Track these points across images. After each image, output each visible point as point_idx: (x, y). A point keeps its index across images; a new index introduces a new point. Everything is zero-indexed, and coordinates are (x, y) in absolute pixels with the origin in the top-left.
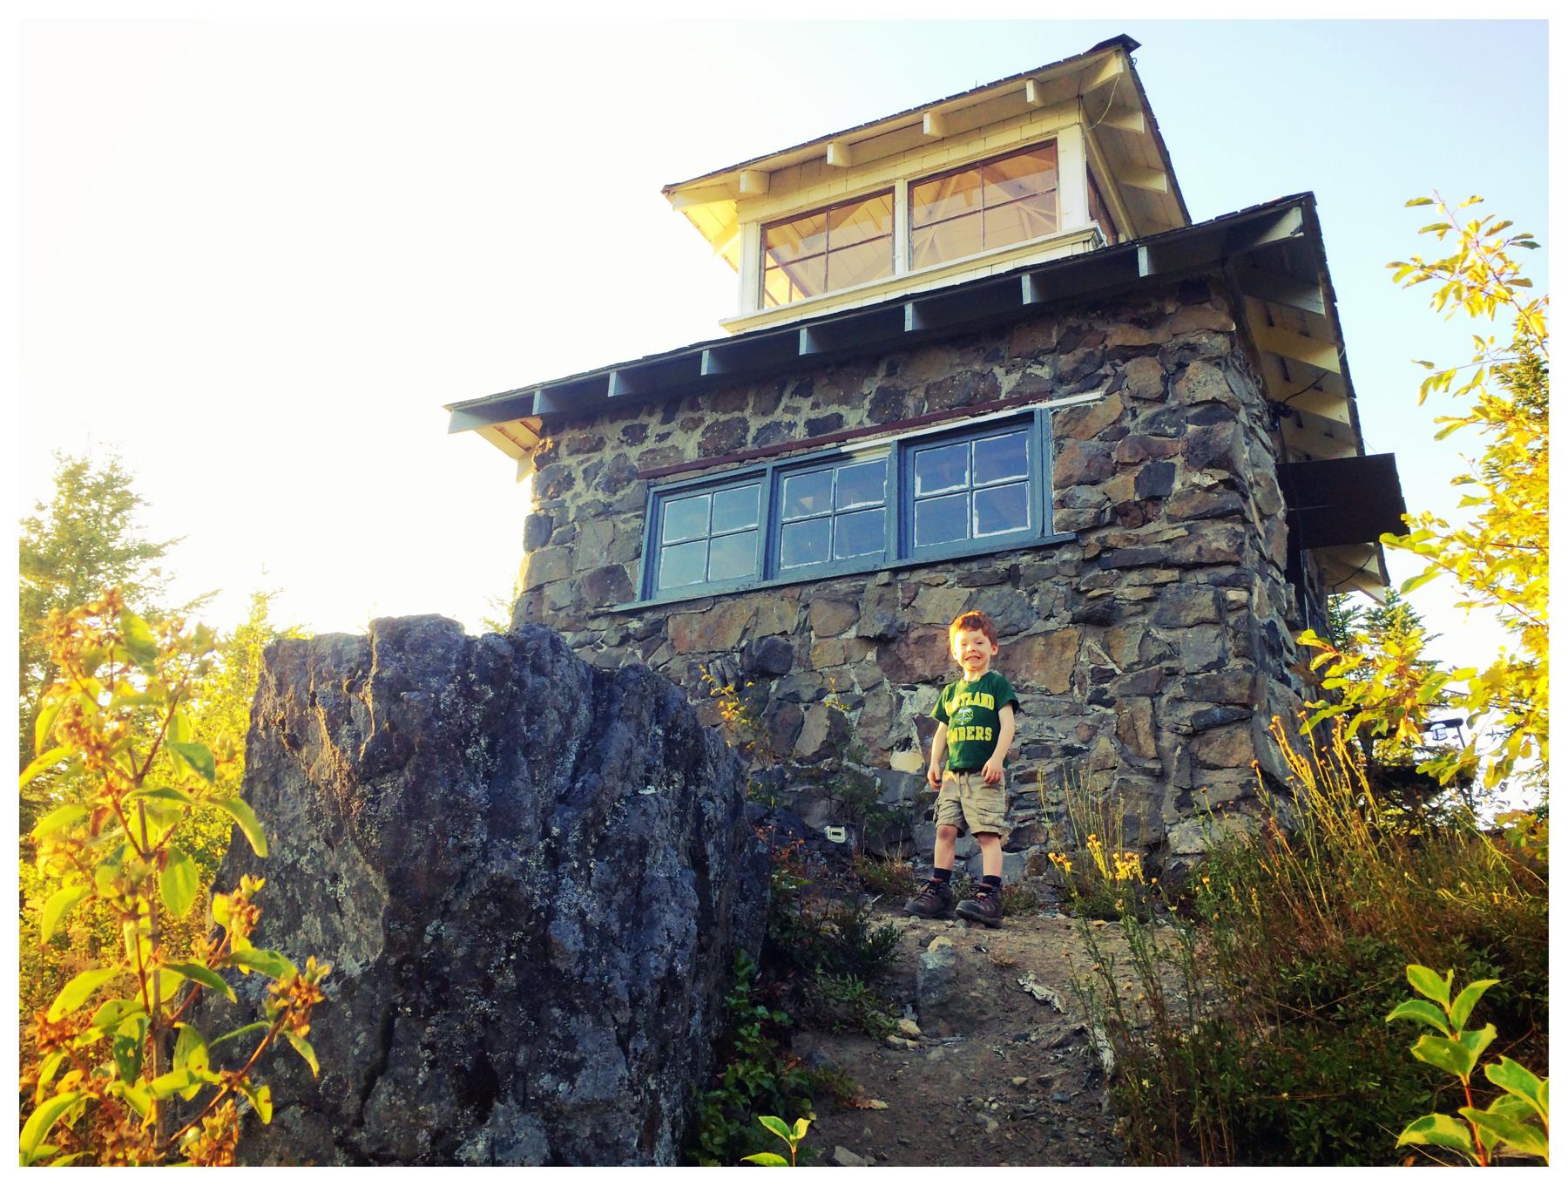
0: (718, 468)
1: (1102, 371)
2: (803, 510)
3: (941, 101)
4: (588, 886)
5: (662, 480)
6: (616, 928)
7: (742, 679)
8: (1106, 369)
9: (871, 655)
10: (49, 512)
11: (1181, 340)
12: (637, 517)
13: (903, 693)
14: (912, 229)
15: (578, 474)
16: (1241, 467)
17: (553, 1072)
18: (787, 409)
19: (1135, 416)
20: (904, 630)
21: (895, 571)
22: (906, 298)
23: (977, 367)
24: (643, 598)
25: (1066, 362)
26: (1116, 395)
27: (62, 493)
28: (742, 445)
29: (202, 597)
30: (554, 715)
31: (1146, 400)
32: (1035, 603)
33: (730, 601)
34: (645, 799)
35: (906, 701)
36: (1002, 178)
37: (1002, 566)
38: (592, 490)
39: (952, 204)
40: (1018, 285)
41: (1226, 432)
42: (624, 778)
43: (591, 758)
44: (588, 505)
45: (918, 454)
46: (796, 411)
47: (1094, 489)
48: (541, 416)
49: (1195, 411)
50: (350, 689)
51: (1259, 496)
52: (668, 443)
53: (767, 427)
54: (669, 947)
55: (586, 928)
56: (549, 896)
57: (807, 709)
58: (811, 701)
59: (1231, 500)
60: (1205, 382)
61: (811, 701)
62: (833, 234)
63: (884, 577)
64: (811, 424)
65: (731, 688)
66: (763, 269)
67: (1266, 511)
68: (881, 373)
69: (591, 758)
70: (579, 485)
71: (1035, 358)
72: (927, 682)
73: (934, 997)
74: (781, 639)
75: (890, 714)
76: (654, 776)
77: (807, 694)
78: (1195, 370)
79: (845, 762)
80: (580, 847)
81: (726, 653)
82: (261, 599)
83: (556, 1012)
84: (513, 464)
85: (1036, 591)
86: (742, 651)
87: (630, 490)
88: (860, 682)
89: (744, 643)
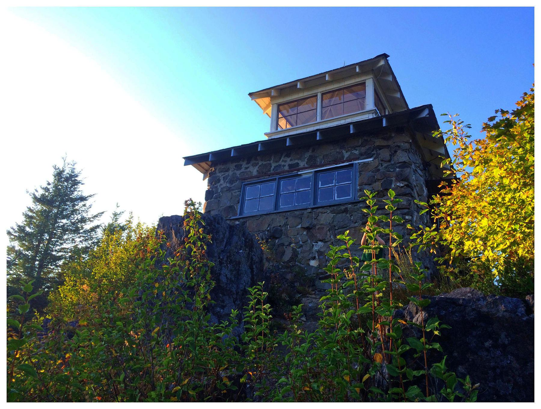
0: (262, 178)
1: (373, 152)
2: (289, 190)
3: (331, 71)
4: (228, 270)
5: (246, 181)
6: (233, 279)
7: (268, 239)
8: (374, 152)
9: (305, 233)
10: (52, 186)
11: (396, 144)
12: (239, 191)
13: (314, 244)
14: (322, 107)
15: (222, 179)
16: (411, 181)
17: (220, 307)
18: (283, 161)
19: (382, 166)
20: (315, 226)
21: (313, 209)
22: (317, 130)
23: (338, 150)
24: (240, 215)
25: (363, 149)
26: (377, 160)
27: (56, 180)
28: (269, 171)
29: (99, 214)
30: (221, 233)
31: (385, 161)
32: (352, 218)
33: (265, 216)
34: (240, 253)
35: (315, 246)
36: (352, 92)
37: (343, 208)
38: (225, 183)
39: (335, 100)
40: (349, 127)
41: (407, 171)
42: (236, 248)
43: (229, 243)
44: (224, 187)
45: (320, 175)
46: (285, 161)
47: (369, 186)
48: (211, 161)
49: (399, 165)
50: (180, 226)
51: (418, 189)
52: (248, 170)
53: (277, 166)
54: (244, 284)
55: (227, 278)
56: (220, 271)
57: (286, 248)
58: (287, 246)
59: (408, 190)
60: (402, 157)
61: (287, 246)
62: (299, 108)
63: (309, 210)
64: (289, 165)
65: (264, 241)
66: (278, 118)
67: (420, 194)
68: (310, 151)
69: (229, 243)
70: (222, 182)
71: (355, 148)
72: (320, 241)
73: (310, 313)
74: (279, 228)
75: (310, 250)
76: (242, 248)
77: (286, 244)
78: (399, 153)
79: (297, 263)
80: (226, 261)
81: (263, 231)
82: (115, 215)
83: (221, 295)
84: (202, 175)
85: (352, 215)
86: (268, 231)
87: (237, 183)
88: (301, 240)
89: (268, 229)
